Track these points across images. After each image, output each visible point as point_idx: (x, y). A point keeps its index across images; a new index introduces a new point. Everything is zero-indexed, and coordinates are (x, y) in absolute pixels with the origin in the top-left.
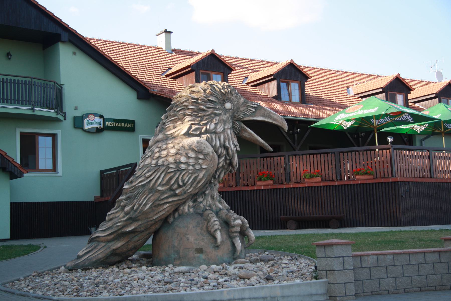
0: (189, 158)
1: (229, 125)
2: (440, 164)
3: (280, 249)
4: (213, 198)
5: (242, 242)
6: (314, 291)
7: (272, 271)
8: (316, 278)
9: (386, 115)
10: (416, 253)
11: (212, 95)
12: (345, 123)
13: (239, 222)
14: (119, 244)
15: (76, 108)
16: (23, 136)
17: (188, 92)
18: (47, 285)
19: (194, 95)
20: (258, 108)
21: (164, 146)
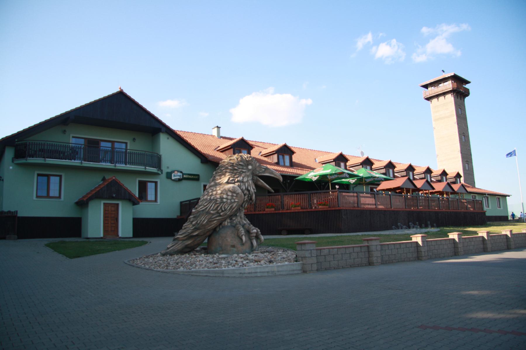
0: (228, 195)
1: (250, 178)
2: (363, 200)
3: (277, 246)
4: (241, 218)
5: (257, 242)
6: (295, 268)
7: (272, 257)
8: (296, 261)
9: (335, 174)
10: (349, 247)
11: (241, 161)
12: (314, 177)
13: (255, 231)
14: (189, 242)
15: (168, 168)
16: (140, 182)
17: (228, 159)
18: (151, 263)
19: (231, 161)
20: (267, 169)
21: (215, 189)
